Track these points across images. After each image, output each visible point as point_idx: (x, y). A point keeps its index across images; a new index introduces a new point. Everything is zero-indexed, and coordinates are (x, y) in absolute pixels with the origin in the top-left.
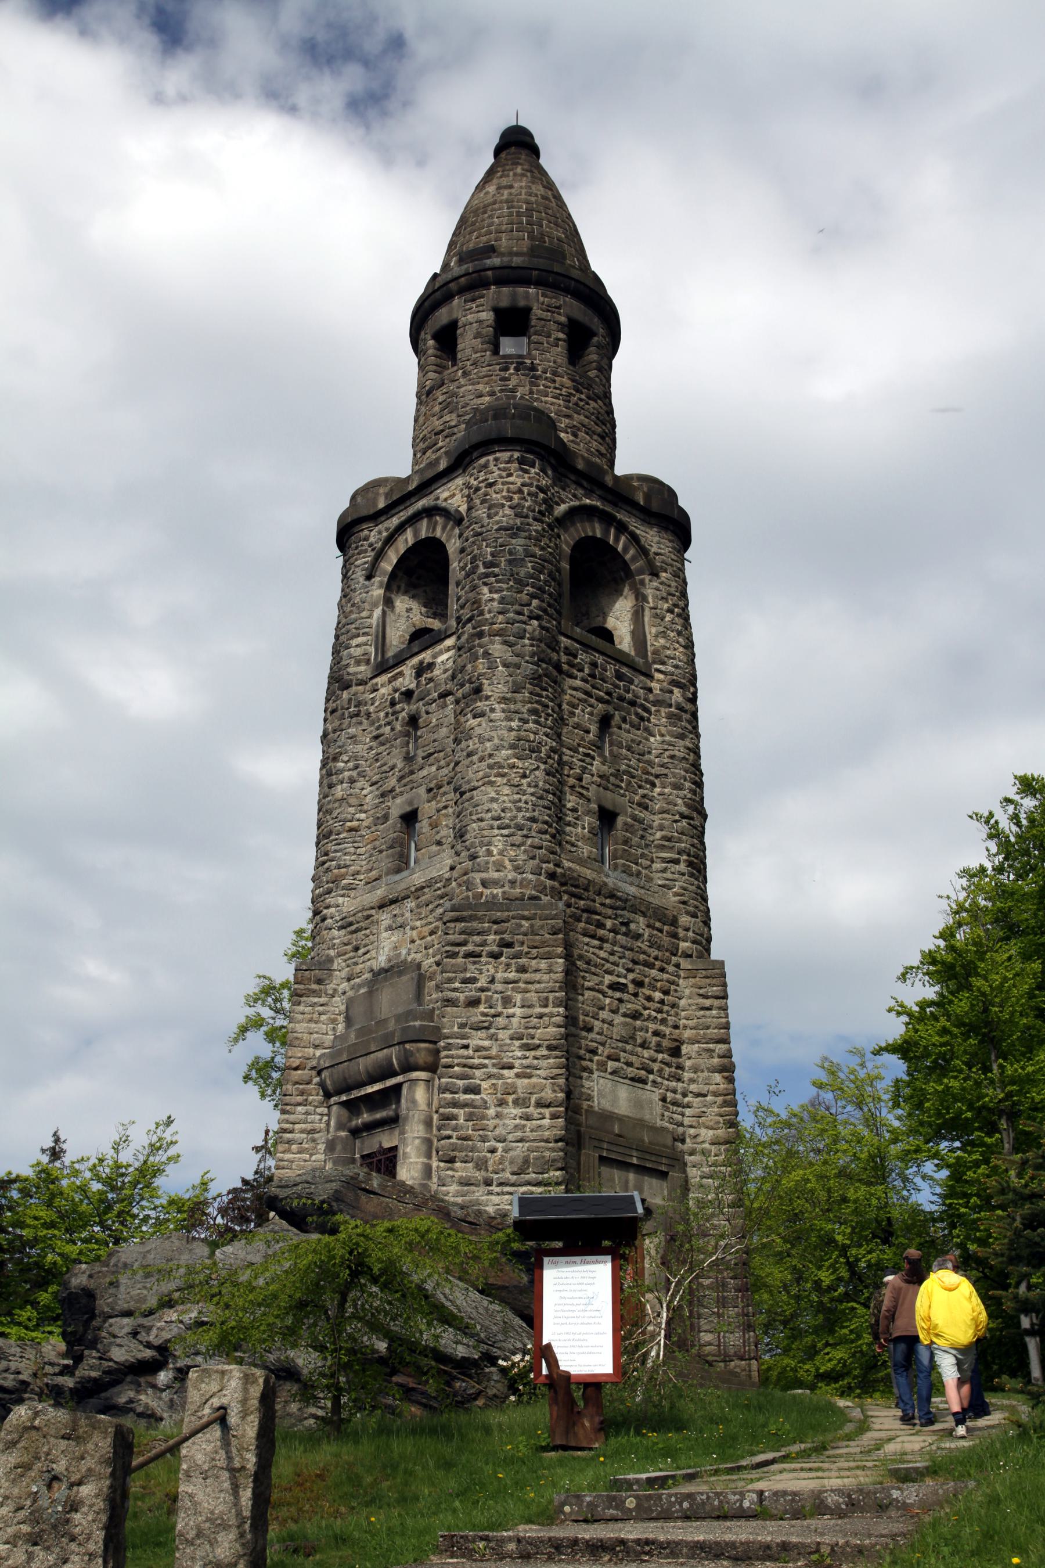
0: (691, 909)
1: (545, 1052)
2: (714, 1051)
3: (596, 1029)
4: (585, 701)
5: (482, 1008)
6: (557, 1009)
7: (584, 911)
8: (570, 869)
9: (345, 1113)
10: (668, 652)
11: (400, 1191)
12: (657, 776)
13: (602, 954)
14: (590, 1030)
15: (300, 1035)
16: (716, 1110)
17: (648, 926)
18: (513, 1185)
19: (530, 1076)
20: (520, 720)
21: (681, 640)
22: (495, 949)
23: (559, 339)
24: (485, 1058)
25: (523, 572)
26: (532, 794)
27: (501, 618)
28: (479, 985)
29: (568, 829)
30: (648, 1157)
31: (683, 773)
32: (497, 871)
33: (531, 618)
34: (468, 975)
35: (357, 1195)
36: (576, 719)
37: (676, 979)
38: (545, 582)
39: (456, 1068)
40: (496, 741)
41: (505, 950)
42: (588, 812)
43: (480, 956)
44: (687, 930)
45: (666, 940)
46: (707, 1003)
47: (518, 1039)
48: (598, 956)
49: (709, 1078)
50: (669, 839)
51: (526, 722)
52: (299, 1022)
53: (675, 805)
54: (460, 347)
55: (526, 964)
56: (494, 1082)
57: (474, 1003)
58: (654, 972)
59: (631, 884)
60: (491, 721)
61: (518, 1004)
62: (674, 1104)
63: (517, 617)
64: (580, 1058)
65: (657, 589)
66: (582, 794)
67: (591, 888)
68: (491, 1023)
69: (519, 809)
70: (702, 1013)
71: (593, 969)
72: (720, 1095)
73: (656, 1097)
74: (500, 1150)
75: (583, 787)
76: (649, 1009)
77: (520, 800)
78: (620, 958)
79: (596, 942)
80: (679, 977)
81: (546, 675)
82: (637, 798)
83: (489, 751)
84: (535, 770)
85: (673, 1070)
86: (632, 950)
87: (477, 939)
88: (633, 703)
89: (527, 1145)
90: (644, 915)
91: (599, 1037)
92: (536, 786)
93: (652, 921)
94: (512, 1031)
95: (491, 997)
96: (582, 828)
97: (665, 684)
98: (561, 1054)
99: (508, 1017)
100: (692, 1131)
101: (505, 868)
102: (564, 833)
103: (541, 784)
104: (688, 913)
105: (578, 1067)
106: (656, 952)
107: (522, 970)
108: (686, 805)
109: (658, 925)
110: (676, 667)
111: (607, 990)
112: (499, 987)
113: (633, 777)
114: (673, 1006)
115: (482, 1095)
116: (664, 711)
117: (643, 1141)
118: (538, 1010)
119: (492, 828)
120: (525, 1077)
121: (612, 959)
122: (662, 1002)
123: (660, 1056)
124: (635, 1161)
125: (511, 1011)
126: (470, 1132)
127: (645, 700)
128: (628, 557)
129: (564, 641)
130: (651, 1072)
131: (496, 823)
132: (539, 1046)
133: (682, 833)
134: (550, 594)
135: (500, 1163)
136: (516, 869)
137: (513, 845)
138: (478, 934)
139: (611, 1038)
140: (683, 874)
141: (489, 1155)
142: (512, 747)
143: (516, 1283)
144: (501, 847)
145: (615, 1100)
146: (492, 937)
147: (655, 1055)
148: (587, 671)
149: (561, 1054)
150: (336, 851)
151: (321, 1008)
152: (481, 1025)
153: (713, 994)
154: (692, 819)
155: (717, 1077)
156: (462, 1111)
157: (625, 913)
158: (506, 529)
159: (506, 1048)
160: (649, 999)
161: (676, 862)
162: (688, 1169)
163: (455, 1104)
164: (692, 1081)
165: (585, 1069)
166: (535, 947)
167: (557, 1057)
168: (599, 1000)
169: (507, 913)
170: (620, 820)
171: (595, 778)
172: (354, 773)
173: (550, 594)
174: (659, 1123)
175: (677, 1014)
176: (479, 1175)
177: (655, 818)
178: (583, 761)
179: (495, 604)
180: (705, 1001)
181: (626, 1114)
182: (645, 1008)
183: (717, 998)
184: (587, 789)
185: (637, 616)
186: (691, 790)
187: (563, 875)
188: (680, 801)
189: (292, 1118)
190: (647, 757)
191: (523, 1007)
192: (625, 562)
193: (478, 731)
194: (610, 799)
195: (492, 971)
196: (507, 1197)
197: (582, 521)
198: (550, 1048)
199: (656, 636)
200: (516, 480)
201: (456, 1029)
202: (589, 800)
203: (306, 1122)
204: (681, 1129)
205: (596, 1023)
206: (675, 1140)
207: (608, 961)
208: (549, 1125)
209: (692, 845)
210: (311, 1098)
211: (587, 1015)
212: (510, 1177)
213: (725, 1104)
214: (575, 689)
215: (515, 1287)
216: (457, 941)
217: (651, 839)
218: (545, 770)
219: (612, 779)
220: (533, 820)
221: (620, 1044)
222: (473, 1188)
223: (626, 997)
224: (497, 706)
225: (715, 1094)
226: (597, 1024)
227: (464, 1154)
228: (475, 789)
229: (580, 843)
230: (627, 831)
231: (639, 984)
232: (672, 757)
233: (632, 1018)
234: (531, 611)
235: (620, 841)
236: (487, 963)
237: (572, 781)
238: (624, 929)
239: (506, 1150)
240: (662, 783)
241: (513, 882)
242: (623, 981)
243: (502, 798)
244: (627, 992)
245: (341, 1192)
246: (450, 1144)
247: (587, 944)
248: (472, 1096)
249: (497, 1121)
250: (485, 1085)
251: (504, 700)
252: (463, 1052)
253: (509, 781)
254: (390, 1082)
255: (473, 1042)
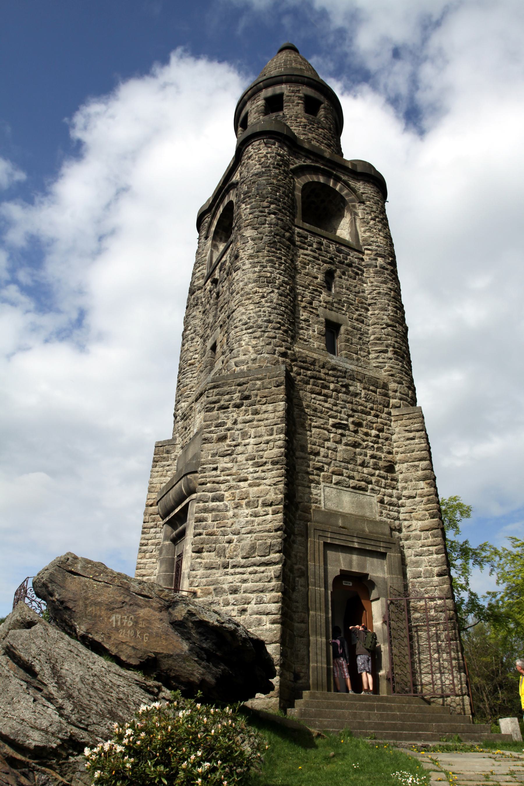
0: (398, 379)
1: (270, 467)
2: (418, 466)
3: (322, 454)
4: (314, 262)
5: (228, 442)
6: (279, 436)
7: (311, 377)
8: (299, 352)
9: (169, 529)
10: (372, 239)
11: (96, 572)
12: (370, 305)
13: (326, 405)
14: (317, 454)
15: (154, 485)
16: (423, 506)
17: (364, 388)
18: (242, 567)
19: (259, 485)
20: (261, 266)
21: (381, 233)
22: (238, 401)
23: (299, 103)
24: (228, 475)
25: (264, 192)
26: (268, 307)
27: (251, 216)
28: (226, 427)
29: (301, 331)
30: (367, 542)
31: (387, 301)
32: (244, 355)
33: (269, 214)
34: (220, 421)
35: (64, 576)
36: (307, 271)
37: (389, 422)
38: (280, 196)
39: (208, 485)
40: (246, 280)
41: (245, 401)
42: (317, 322)
43: (228, 408)
44: (396, 391)
45: (379, 398)
46: (411, 435)
47: (251, 460)
48: (323, 406)
49: (416, 485)
50: (379, 339)
51: (266, 267)
52: (155, 477)
53: (383, 319)
54: (249, 120)
55: (259, 409)
56: (233, 491)
57: (223, 439)
58: (370, 418)
59: (351, 364)
60: (243, 270)
61: (252, 436)
62: (390, 504)
63: (260, 214)
64: (308, 473)
65: (364, 209)
66: (312, 312)
67: (317, 364)
68: (233, 451)
69: (259, 316)
70: (408, 442)
71: (319, 414)
72: (425, 496)
73: (375, 499)
74: (235, 540)
75: (313, 308)
76: (368, 441)
77: (260, 311)
78: (342, 408)
79: (322, 398)
80: (391, 421)
81: (279, 242)
82: (355, 316)
83: (241, 286)
84: (270, 293)
85: (389, 481)
86: (352, 403)
87: (227, 397)
88: (350, 265)
89: (255, 535)
90: (361, 381)
91: (324, 459)
92: (271, 302)
93: (366, 386)
94: (247, 455)
95: (234, 433)
96: (312, 333)
97: (372, 256)
98: (281, 466)
99: (245, 445)
100: (406, 523)
101: (249, 352)
102: (298, 333)
103: (275, 301)
104: (395, 381)
105: (307, 479)
106: (372, 405)
107: (256, 412)
108: (391, 319)
109: (371, 388)
110: (378, 246)
111: (331, 428)
112: (239, 426)
113: (352, 304)
114: (387, 439)
115: (225, 502)
116: (371, 270)
117: (364, 531)
118: (266, 438)
119: (242, 330)
120: (255, 486)
121: (335, 408)
122: (377, 436)
123: (377, 472)
124: (356, 545)
125: (247, 441)
126: (215, 529)
127: (359, 264)
128: (343, 193)
129: (297, 230)
130: (370, 483)
131: (244, 327)
132: (266, 463)
133: (388, 335)
134: (285, 203)
135: (235, 551)
136: (257, 352)
137: (255, 338)
138: (228, 394)
139: (336, 460)
140: (391, 359)
141: (227, 545)
142: (255, 281)
143: (178, 651)
144: (247, 340)
145: (340, 502)
146: (237, 394)
147: (373, 471)
148: (315, 246)
149: (281, 466)
150: (183, 378)
151: (168, 468)
152: (226, 452)
153: (415, 429)
154: (396, 327)
155: (422, 484)
156: (210, 515)
157: (346, 380)
158: (256, 174)
159: (242, 467)
160: (367, 434)
161: (386, 352)
162: (405, 550)
163: (206, 510)
164: (405, 488)
165: (312, 481)
166: (265, 397)
167: (278, 469)
168: (324, 434)
169: (247, 378)
170: (342, 329)
171: (322, 303)
172: (193, 335)
173: (285, 203)
174: (378, 518)
175: (390, 445)
176: (220, 561)
177: (370, 328)
178: (313, 293)
179: (248, 210)
180: (410, 434)
181: (349, 512)
182: (364, 441)
183: (418, 431)
184: (316, 309)
185: (353, 223)
186: (392, 311)
187: (294, 355)
188: (385, 317)
189: (147, 536)
190: (361, 294)
191: (255, 437)
192: (342, 196)
193: (237, 278)
194: (334, 316)
195: (235, 416)
196: (238, 576)
197: (310, 174)
198: (274, 463)
199: (365, 232)
200: (264, 151)
201: (210, 458)
202: (318, 315)
203: (155, 538)
204: (397, 522)
205: (322, 449)
206: (392, 530)
207: (332, 410)
208: (273, 519)
209: (396, 342)
210: (159, 523)
211: (314, 444)
212: (241, 560)
213: (429, 501)
214: (305, 255)
215: (178, 655)
216: (214, 400)
217: (367, 340)
218: (278, 293)
219: (335, 305)
220: (269, 321)
221: (343, 464)
222: (214, 571)
223: (347, 433)
224: (247, 262)
225: (422, 496)
226: (323, 451)
227: (208, 546)
228: (234, 311)
229: (311, 340)
230: (348, 334)
231: (359, 425)
232: (379, 293)
233: (352, 446)
234: (270, 210)
235: (343, 340)
236: (232, 412)
237: (303, 304)
238: (344, 389)
239: (239, 541)
240: (373, 308)
241: (254, 360)
242: (345, 422)
243: (248, 312)
244: (349, 430)
245: (54, 575)
246: (200, 539)
247: (314, 399)
248: (218, 503)
249: (234, 519)
250: (227, 494)
251: (251, 256)
252: (214, 473)
253: (253, 301)
254: (184, 504)
255: (220, 466)
